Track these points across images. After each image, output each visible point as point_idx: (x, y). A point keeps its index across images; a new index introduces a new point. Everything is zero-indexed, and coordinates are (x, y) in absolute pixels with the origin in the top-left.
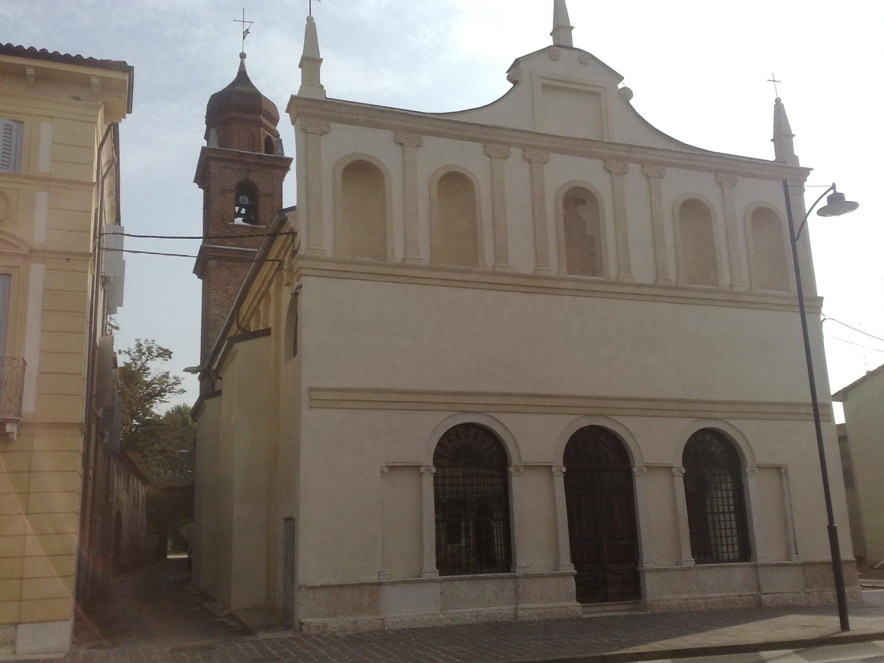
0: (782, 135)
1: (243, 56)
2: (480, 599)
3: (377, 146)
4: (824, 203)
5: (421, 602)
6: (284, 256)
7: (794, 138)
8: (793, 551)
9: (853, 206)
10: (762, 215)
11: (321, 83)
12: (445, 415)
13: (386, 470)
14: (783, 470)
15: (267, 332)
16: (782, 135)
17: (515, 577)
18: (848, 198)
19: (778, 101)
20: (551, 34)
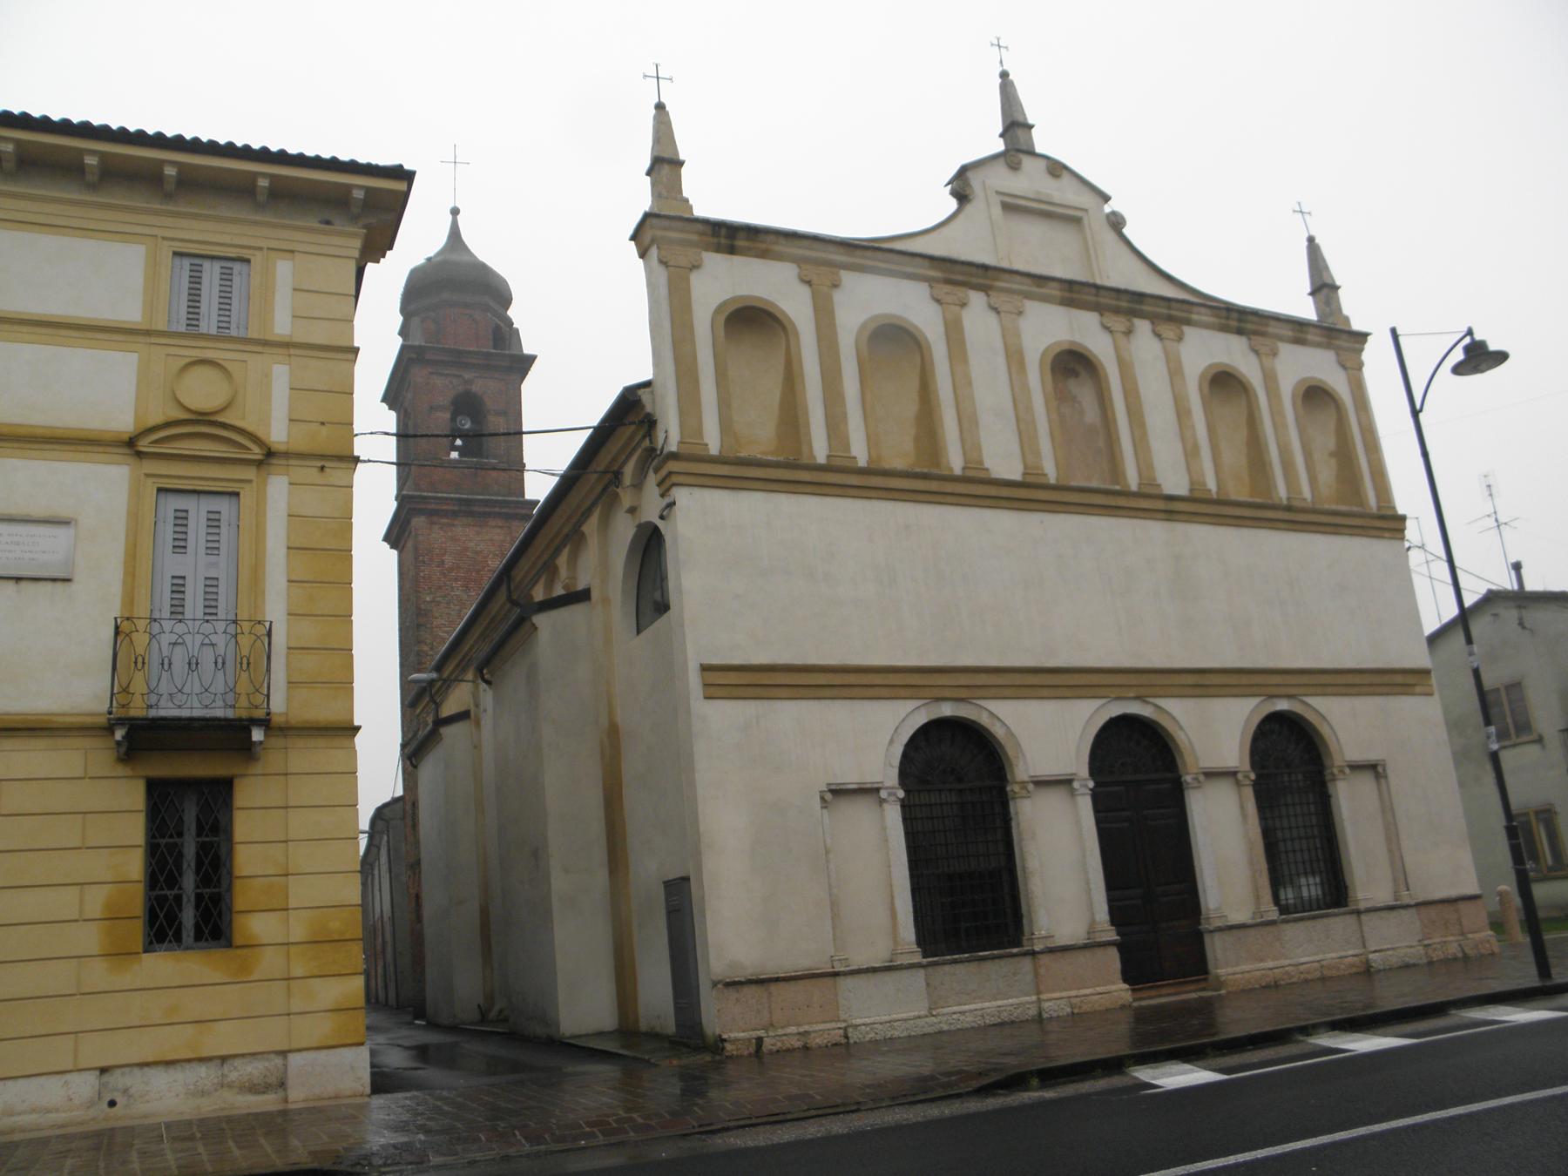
0: (1323, 288)
1: (455, 212)
2: (981, 998)
3: (775, 283)
4: (1458, 355)
5: (908, 1006)
6: (625, 463)
7: (1340, 292)
8: (1402, 887)
9: (1502, 357)
10: (1315, 395)
11: (685, 194)
12: (910, 705)
13: (829, 796)
14: (1380, 769)
15: (583, 596)
16: (1323, 288)
17: (1033, 953)
18: (1493, 347)
19: (1311, 240)
20: (1002, 136)
